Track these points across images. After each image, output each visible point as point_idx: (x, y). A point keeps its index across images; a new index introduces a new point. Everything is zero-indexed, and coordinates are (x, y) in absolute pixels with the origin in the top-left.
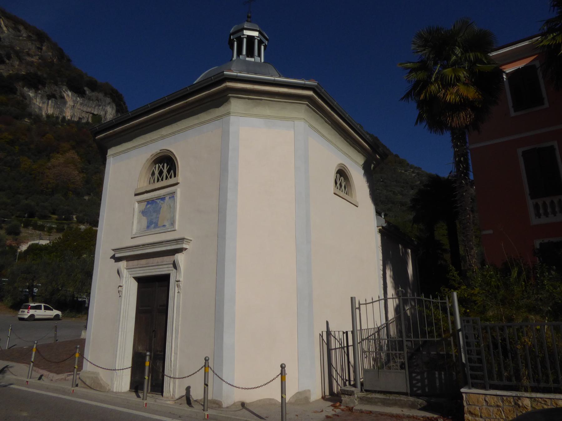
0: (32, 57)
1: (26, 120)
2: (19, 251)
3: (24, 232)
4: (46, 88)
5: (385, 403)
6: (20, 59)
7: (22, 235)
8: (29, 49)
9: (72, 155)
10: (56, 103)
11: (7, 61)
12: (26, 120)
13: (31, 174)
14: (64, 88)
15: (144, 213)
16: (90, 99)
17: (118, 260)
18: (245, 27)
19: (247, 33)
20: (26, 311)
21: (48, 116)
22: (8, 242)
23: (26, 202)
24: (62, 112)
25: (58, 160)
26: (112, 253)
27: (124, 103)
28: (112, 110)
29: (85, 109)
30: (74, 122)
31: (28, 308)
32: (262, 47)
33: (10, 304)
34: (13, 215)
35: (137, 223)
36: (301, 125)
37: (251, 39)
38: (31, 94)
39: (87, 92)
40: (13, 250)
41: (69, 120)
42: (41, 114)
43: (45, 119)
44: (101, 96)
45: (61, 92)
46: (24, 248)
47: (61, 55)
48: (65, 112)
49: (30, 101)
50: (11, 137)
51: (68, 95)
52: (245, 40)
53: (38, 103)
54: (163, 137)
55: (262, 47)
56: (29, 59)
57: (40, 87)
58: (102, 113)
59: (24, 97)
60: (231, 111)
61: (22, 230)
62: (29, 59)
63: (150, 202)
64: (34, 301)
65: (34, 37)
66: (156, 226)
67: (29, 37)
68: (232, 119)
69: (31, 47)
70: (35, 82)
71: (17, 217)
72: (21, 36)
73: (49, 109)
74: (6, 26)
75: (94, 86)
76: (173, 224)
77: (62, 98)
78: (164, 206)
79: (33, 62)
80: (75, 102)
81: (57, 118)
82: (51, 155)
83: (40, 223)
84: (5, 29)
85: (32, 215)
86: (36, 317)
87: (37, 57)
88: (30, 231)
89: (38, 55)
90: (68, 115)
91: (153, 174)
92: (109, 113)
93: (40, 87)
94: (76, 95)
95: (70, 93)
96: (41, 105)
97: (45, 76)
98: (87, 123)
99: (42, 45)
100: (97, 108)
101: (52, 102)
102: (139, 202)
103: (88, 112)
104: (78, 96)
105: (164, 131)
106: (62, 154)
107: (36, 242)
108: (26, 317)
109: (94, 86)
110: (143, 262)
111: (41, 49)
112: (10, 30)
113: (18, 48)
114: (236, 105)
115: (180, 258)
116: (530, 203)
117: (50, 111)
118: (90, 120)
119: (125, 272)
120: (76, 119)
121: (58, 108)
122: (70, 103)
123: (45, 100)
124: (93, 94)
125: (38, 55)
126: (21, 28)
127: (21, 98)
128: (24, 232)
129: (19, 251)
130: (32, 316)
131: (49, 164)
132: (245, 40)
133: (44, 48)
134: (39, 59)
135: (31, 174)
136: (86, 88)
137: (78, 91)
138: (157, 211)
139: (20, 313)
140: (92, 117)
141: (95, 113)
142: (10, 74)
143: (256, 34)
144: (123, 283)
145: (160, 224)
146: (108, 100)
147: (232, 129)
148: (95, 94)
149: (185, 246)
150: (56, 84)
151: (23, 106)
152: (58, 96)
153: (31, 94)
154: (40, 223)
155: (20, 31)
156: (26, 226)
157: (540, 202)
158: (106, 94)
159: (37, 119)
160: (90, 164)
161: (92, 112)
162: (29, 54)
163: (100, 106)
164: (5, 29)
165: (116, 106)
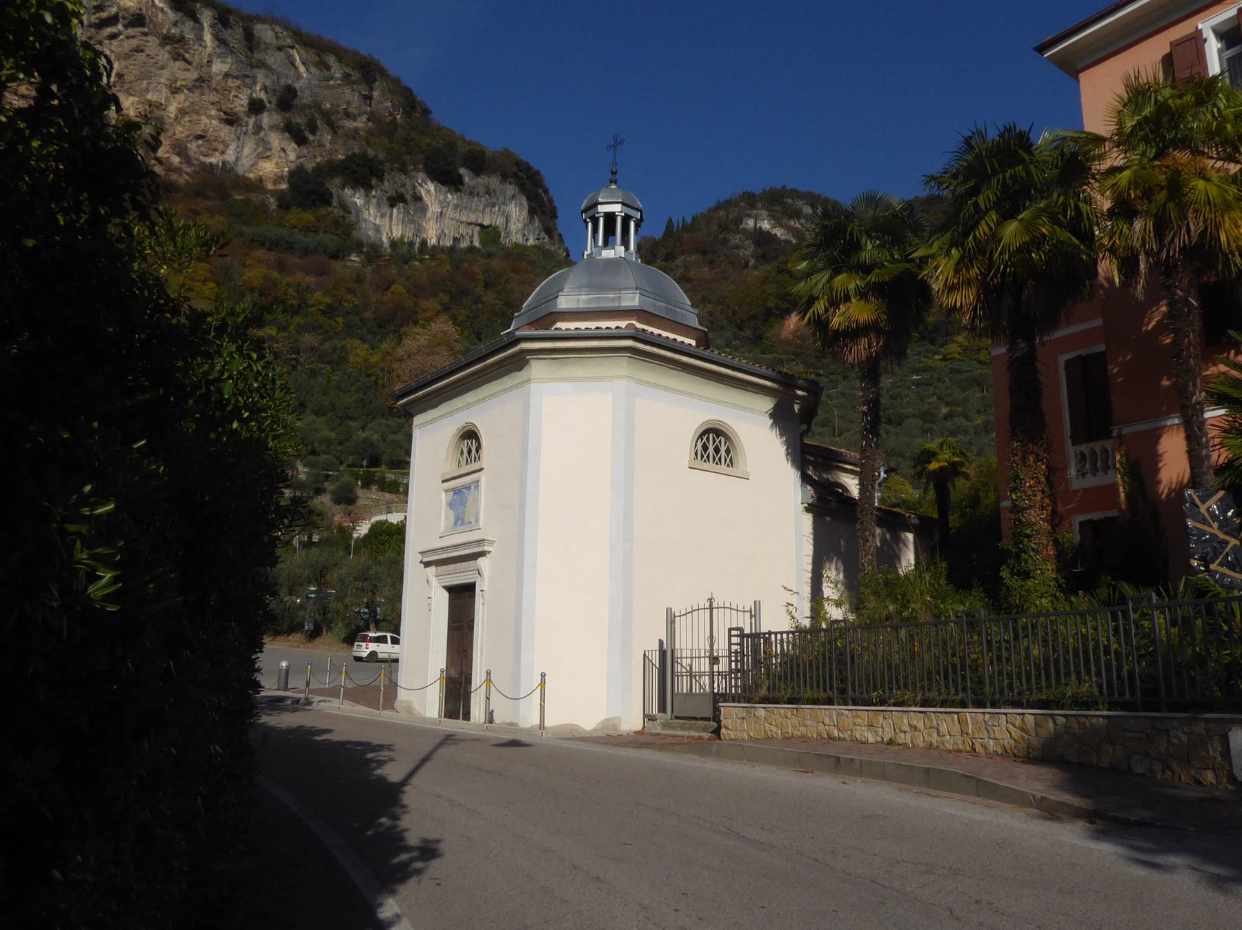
0: (355, 119)
1: (354, 257)
2: (355, 535)
3: (366, 496)
4: (386, 183)
5: (682, 728)
6: (333, 128)
7: (360, 502)
8: (348, 103)
9: (443, 326)
10: (407, 212)
11: (311, 138)
12: (354, 257)
13: (368, 376)
14: (421, 176)
15: (451, 505)
16: (472, 193)
17: (427, 564)
18: (600, 200)
19: (603, 209)
20: (364, 644)
21: (394, 244)
22: (337, 518)
23: (364, 435)
24: (419, 230)
25: (416, 339)
26: (420, 557)
27: (546, 191)
28: (521, 211)
29: (464, 219)
30: (443, 250)
31: (365, 639)
32: (632, 224)
33: (343, 636)
34: (341, 463)
35: (444, 517)
36: (621, 385)
37: (610, 217)
38: (359, 201)
39: (466, 179)
40: (345, 533)
41: (434, 246)
42: (380, 240)
43: (389, 250)
44: (494, 182)
45: (414, 187)
46: (363, 529)
47: (409, 102)
48: (425, 230)
49: (358, 216)
50: (327, 300)
51: (429, 190)
52: (601, 220)
53: (371, 219)
54: (468, 406)
55: (632, 224)
56: (349, 124)
57: (374, 181)
58: (500, 221)
59: (345, 207)
60: (533, 376)
61: (361, 493)
62: (349, 124)
63: (457, 491)
64: (378, 629)
65: (356, 75)
66: (463, 524)
67: (347, 76)
68: (533, 386)
69: (351, 97)
70: (362, 173)
71: (349, 466)
72: (332, 78)
73: (394, 228)
74: (304, 64)
75: (478, 162)
76: (477, 521)
77: (418, 198)
78: (470, 496)
79: (356, 130)
80: (444, 204)
81: (411, 244)
82: (403, 330)
83: (390, 476)
84: (302, 69)
85: (375, 462)
86: (380, 656)
87: (364, 118)
88: (374, 494)
89: (365, 113)
90: (431, 235)
91: (462, 453)
92: (514, 220)
93: (374, 181)
94: (444, 189)
95: (431, 186)
96: (377, 222)
97: (381, 156)
98: (471, 249)
99: (371, 89)
100: (488, 210)
101: (399, 212)
102: (446, 491)
103: (470, 224)
104: (449, 191)
105: (471, 397)
106: (423, 327)
107: (382, 517)
108: (364, 655)
109: (478, 162)
110: (451, 567)
111: (370, 98)
112: (312, 69)
113: (328, 106)
114: (537, 368)
115: (482, 562)
116: (1071, 450)
117: (397, 233)
118: (477, 244)
119: (434, 580)
120: (448, 243)
121: (411, 222)
122: (434, 208)
123: (386, 210)
124: (479, 180)
125: (365, 113)
126: (331, 60)
127: (342, 213)
128: (366, 496)
129: (355, 535)
130: (373, 654)
131: (400, 351)
132: (601, 220)
133: (376, 94)
134: (369, 120)
135: (368, 376)
136: (462, 171)
137: (448, 179)
138: (463, 503)
139: (355, 648)
140: (480, 233)
141: (486, 223)
142: (318, 164)
143: (617, 208)
144: (432, 594)
145: (466, 520)
146: (511, 189)
147: (533, 400)
148: (483, 180)
149: (486, 549)
150: (403, 170)
151: (345, 226)
152: (408, 197)
153: (359, 201)
154: (390, 476)
155: (328, 68)
156: (366, 485)
157: (1084, 448)
158: (504, 177)
159: (373, 253)
160: (480, 340)
161: (480, 221)
162: (348, 115)
163: (494, 205)
164: (302, 69)
165: (528, 200)
